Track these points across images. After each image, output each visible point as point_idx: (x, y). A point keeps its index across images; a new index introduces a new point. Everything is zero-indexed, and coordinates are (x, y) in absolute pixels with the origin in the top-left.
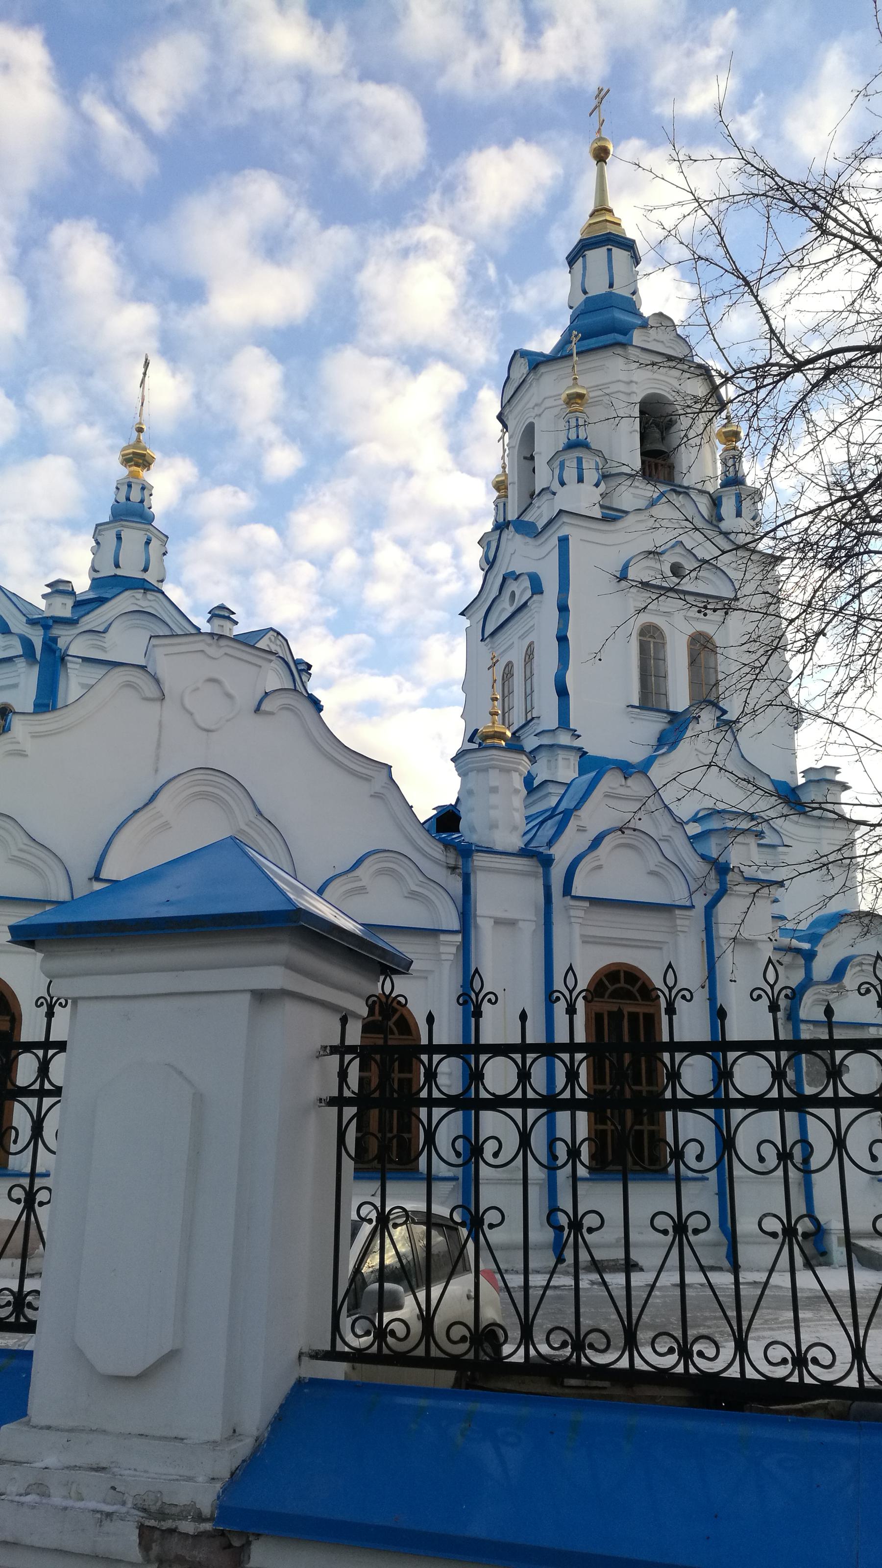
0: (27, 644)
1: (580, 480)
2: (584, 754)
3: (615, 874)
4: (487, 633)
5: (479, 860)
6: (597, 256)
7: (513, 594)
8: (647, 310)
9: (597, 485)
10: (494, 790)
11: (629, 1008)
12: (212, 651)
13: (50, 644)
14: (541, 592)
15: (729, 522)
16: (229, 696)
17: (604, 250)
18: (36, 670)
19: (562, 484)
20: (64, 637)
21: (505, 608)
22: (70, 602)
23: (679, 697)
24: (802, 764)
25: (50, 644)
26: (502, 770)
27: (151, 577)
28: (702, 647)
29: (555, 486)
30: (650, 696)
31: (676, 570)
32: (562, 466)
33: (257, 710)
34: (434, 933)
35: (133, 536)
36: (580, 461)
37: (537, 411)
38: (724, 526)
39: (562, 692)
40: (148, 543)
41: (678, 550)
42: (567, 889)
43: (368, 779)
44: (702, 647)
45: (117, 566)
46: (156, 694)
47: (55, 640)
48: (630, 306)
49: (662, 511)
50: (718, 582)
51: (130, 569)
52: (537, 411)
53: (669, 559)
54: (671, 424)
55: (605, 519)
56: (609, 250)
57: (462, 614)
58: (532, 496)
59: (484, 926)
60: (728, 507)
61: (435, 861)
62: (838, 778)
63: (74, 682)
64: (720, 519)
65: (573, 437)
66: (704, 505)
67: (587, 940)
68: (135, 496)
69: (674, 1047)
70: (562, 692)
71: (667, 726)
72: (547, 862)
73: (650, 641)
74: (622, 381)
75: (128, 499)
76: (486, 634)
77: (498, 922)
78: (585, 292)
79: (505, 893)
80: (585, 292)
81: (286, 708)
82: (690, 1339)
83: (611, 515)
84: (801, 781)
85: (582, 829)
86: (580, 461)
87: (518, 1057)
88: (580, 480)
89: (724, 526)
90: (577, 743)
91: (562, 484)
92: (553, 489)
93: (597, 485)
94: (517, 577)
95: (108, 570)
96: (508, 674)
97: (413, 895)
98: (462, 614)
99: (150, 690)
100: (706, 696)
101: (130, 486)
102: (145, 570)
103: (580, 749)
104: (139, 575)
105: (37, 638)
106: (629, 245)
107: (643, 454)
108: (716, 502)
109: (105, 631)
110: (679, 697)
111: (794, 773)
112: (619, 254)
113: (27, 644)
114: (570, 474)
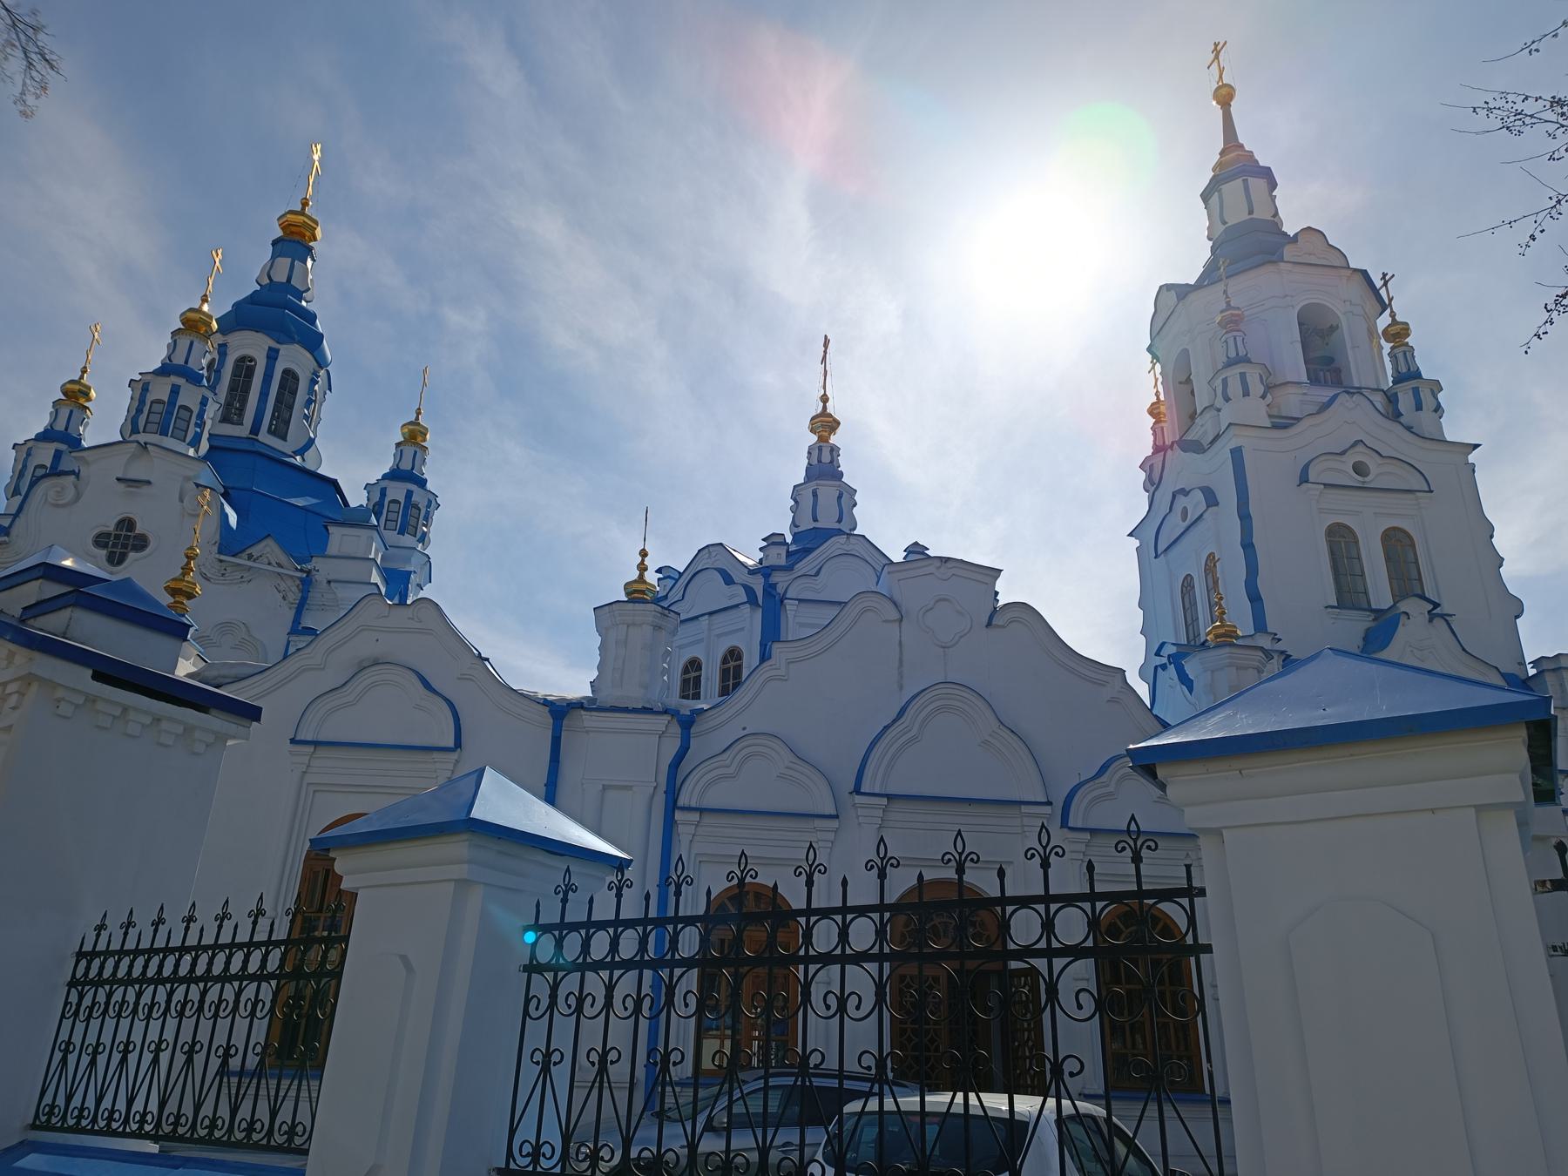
0: (749, 591)
1: (1246, 393)
4: (1161, 548)
8: (1290, 228)
9: (1263, 397)
13: (770, 589)
17: (1239, 182)
18: (759, 614)
19: (1227, 399)
20: (779, 579)
21: (1175, 525)
22: (783, 551)
23: (1381, 593)
24: (1530, 655)
25: (770, 589)
27: (844, 527)
28: (1397, 544)
29: (1219, 402)
30: (1349, 594)
31: (1360, 469)
33: (989, 624)
35: (827, 492)
36: (1243, 376)
39: (1255, 598)
40: (840, 497)
45: (815, 520)
46: (895, 615)
47: (774, 586)
48: (1274, 225)
51: (827, 521)
53: (1351, 458)
54: (1333, 329)
55: (1275, 427)
56: (1245, 181)
57: (1130, 535)
58: (1193, 416)
63: (795, 619)
66: (1378, 399)
68: (826, 458)
69: (880, 958)
71: (1372, 624)
73: (1341, 541)
74: (1272, 298)
76: (1161, 548)
78: (1224, 223)
80: (1224, 223)
82: (806, 1160)
84: (1532, 672)
87: (1087, 906)
88: (1246, 393)
91: (1227, 399)
92: (1218, 405)
93: (1263, 397)
94: (1184, 492)
95: (807, 524)
96: (1188, 584)
98: (1130, 535)
100: (1406, 578)
101: (820, 449)
102: (839, 521)
103: (1283, 652)
104: (837, 526)
105: (758, 584)
106: (1267, 174)
108: (1391, 398)
109: (817, 574)
110: (1381, 593)
111: (1522, 663)
112: (1258, 184)
113: (749, 591)
114: (1235, 388)
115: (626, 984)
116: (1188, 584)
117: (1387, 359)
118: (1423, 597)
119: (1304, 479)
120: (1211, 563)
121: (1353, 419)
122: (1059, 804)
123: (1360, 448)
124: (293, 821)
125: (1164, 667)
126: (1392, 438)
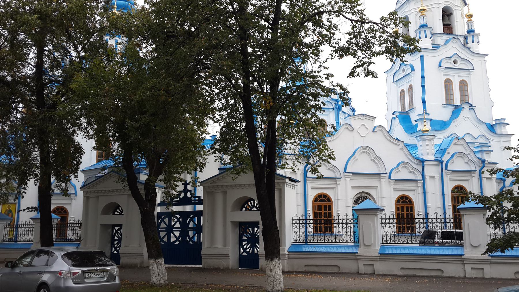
2: (431, 120)
3: (458, 164)
5: (425, 163)
7: (404, 70)
10: (427, 145)
11: (464, 196)
12: (362, 118)
14: (414, 70)
15: (470, 44)
16: (367, 128)
26: (429, 140)
28: (463, 84)
30: (449, 101)
31: (455, 62)
32: (420, 32)
33: (373, 131)
34: (416, 181)
37: (409, 13)
38: (468, 46)
39: (424, 102)
41: (456, 56)
42: (446, 168)
43: (399, 145)
44: (463, 84)
49: (450, 45)
50: (468, 65)
52: (409, 13)
59: (427, 179)
60: (470, 40)
61: (415, 163)
62: (505, 122)
64: (467, 43)
65: (423, 23)
66: (462, 40)
67: (451, 180)
70: (424, 102)
72: (442, 162)
73: (448, 83)
77: (431, 177)
79: (432, 171)
81: (379, 130)
83: (436, 47)
85: (449, 153)
86: (425, 31)
88: (426, 37)
89: (468, 46)
90: (429, 117)
96: (403, 92)
97: (411, 172)
99: (351, 129)
100: (465, 100)
107: (443, 25)
108: (466, 38)
110: (457, 101)
114: (423, 35)
115: (422, 225)
116: (403, 92)
117: (466, 24)
118: (468, 103)
119: (440, 66)
120: (411, 87)
121: (453, 48)
122: (388, 173)
123: (456, 56)
124: (469, 228)
125: (395, 118)
126: (464, 54)
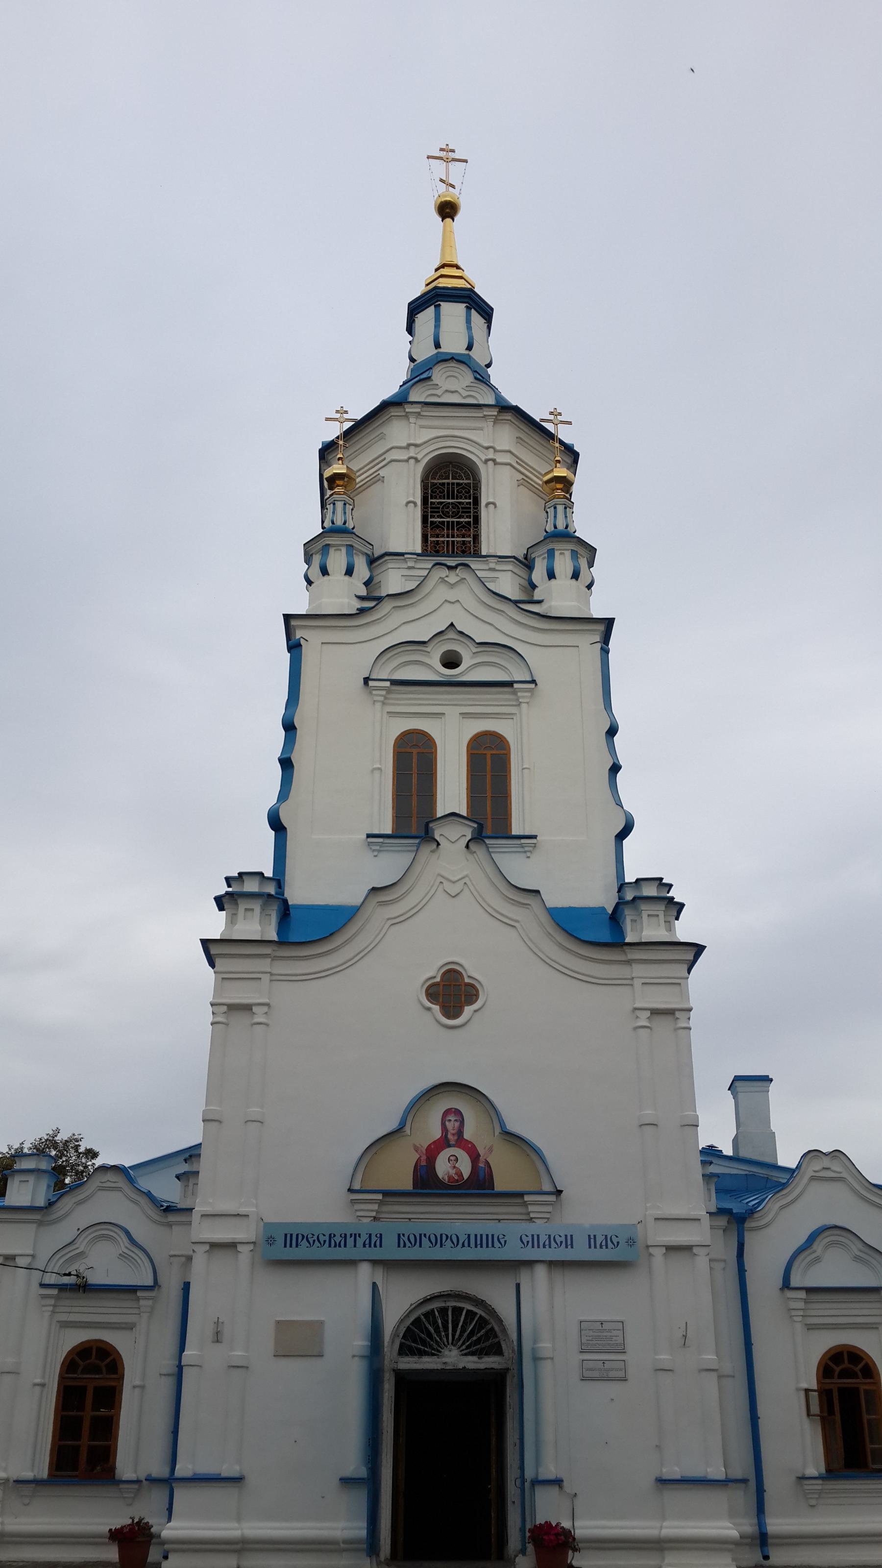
6: (426, 317)
73: (414, 759)
75: (555, 527)
88: (551, 575)
